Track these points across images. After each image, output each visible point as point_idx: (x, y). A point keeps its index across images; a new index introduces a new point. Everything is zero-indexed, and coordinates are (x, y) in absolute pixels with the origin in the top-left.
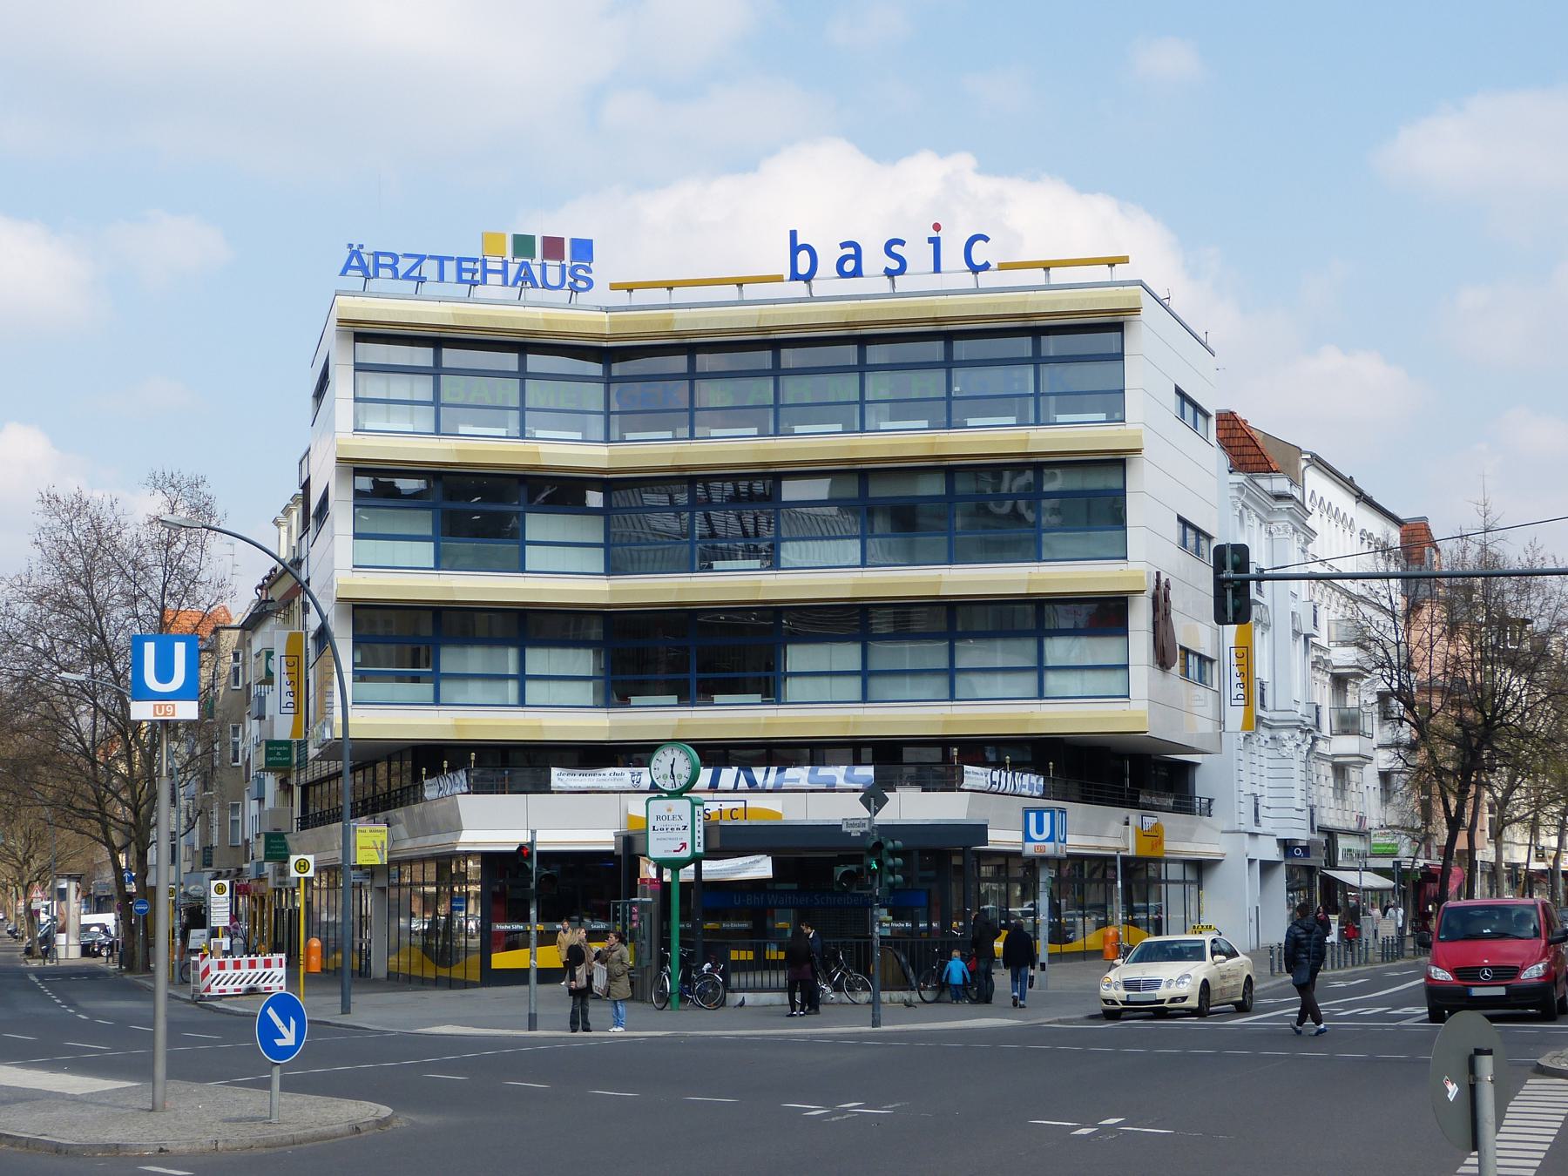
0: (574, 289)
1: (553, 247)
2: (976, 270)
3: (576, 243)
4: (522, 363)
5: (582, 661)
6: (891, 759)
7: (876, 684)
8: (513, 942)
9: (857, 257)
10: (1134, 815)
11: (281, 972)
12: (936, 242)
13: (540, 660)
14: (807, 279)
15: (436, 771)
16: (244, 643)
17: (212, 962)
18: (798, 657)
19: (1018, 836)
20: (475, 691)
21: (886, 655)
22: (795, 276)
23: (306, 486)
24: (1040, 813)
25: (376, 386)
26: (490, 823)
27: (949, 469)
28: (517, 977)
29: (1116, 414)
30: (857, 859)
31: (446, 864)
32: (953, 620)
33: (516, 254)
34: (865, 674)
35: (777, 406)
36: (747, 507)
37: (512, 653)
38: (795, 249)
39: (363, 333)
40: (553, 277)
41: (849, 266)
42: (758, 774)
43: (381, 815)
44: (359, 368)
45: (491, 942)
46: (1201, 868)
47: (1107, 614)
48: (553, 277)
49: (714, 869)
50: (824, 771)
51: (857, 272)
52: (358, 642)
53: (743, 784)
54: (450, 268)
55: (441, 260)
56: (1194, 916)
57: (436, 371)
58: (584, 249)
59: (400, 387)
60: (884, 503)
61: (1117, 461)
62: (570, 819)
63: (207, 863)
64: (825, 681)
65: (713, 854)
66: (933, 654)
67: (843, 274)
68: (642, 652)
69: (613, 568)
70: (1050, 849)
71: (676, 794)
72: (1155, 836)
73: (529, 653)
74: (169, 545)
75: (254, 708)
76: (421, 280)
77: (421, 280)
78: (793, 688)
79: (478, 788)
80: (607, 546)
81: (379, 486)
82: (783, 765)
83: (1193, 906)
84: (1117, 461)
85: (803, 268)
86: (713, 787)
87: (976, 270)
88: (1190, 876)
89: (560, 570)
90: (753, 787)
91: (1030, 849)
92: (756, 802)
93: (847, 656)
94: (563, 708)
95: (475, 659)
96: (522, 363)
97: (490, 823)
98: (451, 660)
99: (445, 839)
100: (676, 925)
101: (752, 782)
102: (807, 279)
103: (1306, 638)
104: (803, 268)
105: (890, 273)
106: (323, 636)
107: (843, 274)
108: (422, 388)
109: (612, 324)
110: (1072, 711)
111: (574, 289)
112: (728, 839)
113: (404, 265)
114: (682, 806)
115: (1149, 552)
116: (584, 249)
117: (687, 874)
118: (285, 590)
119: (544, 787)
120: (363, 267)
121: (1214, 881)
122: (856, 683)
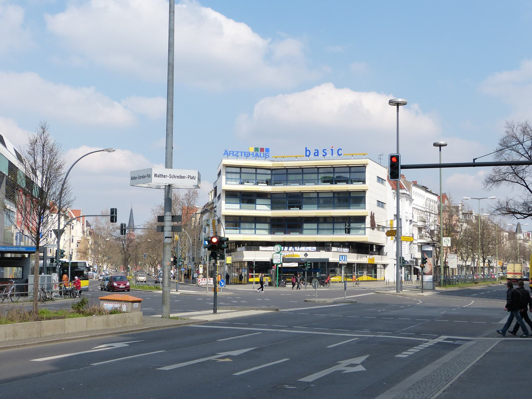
0: (266, 157)
1: (262, 150)
2: (339, 155)
3: (261, 149)
4: (256, 171)
5: (267, 226)
6: (321, 246)
7: (319, 231)
8: (252, 277)
9: (318, 152)
10: (368, 256)
11: (212, 281)
12: (332, 150)
13: (258, 226)
14: (309, 156)
15: (240, 246)
16: (201, 217)
17: (200, 279)
18: (306, 226)
19: (339, 260)
20: (247, 231)
21: (321, 226)
22: (306, 156)
23: (216, 188)
24: (342, 256)
25: (230, 176)
26: (250, 256)
27: (334, 193)
28: (252, 283)
29: (364, 182)
30: (303, 264)
31: (242, 263)
32: (333, 220)
33: (255, 151)
34: (318, 229)
35: (302, 180)
36: (295, 200)
37: (254, 224)
38: (306, 151)
39: (227, 166)
40: (262, 155)
41: (316, 154)
42: (296, 248)
43: (230, 254)
44: (227, 172)
45: (248, 277)
46: (385, 266)
47: (361, 219)
48: (262, 155)
49: (285, 265)
50: (307, 248)
51: (318, 155)
52: (226, 222)
53: (293, 250)
54: (243, 154)
55: (242, 152)
56: (383, 274)
57: (240, 173)
58: (268, 150)
59: (234, 176)
60: (320, 200)
61: (364, 192)
62: (262, 255)
63: (193, 261)
64: (311, 230)
65: (283, 262)
66: (330, 226)
67: (315, 155)
68: (277, 224)
69: (273, 208)
70: (344, 262)
71: (278, 253)
72: (373, 260)
73: (257, 224)
74: (189, 200)
75: (203, 230)
76: (238, 156)
77: (238, 156)
78: (304, 231)
79: (247, 250)
80: (271, 205)
81: (231, 195)
82: (300, 246)
83: (383, 273)
84: (364, 192)
85: (308, 154)
86: (288, 250)
87: (339, 155)
88: (382, 267)
89: (263, 210)
90: (295, 251)
91: (340, 262)
92: (295, 253)
93: (315, 226)
94: (263, 235)
95: (247, 225)
96: (256, 171)
97: (250, 256)
98: (242, 225)
99: (241, 259)
100: (278, 274)
101: (294, 249)
102: (309, 156)
103: (411, 221)
104: (308, 154)
105: (324, 156)
106: (219, 221)
107: (315, 155)
108: (238, 176)
109: (273, 164)
110: (354, 237)
111: (266, 157)
112: (285, 260)
113: (234, 154)
114: (279, 255)
115: (369, 208)
116: (268, 150)
117: (279, 266)
118: (210, 209)
119: (258, 250)
120: (227, 154)
121: (387, 268)
122: (316, 231)
